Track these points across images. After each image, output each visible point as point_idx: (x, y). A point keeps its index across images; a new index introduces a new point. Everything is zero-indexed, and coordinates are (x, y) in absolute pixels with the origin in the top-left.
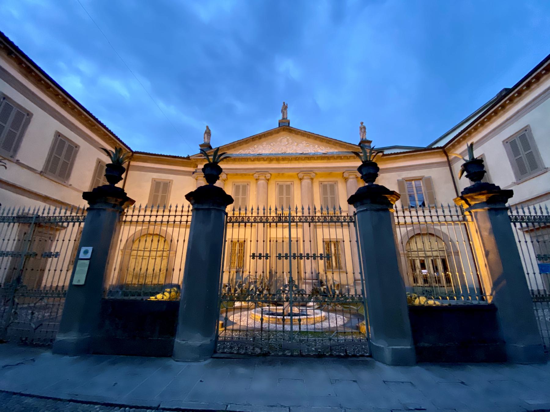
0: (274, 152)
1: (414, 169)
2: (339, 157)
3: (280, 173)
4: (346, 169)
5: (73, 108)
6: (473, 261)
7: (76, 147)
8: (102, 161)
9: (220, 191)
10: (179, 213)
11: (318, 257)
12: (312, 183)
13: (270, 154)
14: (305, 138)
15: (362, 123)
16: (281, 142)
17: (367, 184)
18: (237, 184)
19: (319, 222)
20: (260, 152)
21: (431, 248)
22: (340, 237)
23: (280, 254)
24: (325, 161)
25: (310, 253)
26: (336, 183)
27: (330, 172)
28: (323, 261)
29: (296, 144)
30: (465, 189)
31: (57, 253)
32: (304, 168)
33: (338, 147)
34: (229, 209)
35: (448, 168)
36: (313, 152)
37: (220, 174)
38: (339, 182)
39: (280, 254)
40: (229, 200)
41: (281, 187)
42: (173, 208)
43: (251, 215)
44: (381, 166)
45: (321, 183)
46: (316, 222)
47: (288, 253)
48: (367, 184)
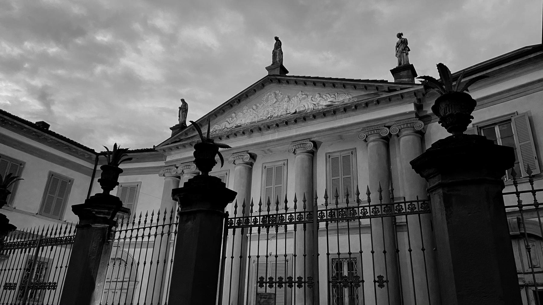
0: (256, 120)
1: (494, 103)
2: (356, 107)
4: (364, 125)
6: (387, 300)
7: (21, 165)
8: (56, 173)
9: (218, 184)
10: (142, 226)
11: (285, 283)
13: (251, 123)
14: (300, 87)
15: (400, 35)
16: (267, 101)
19: (364, 217)
20: (238, 123)
21: (533, 267)
22: (355, 249)
23: (262, 278)
24: (328, 118)
25: (274, 277)
26: (353, 151)
27: (339, 135)
28: (385, 289)
29: (286, 99)
30: (121, 202)
33: (351, 91)
34: (229, 208)
35: (90, 178)
36: (311, 107)
38: (358, 150)
39: (290, 278)
41: (269, 171)
45: (328, 156)
46: (360, 218)
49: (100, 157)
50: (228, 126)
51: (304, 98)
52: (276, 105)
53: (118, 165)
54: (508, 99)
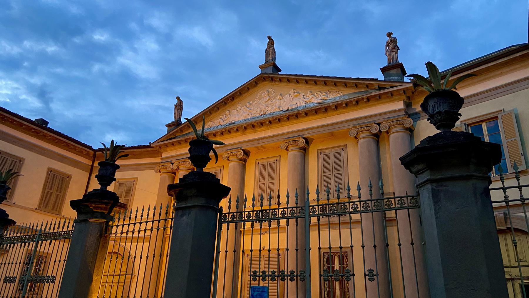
2: (347, 105)
3: (261, 146)
5: (12, 122)
7: (20, 161)
10: (138, 221)
12: (244, 166)
13: (245, 120)
17: (440, 131)
18: (262, 162)
19: (355, 212)
20: (232, 120)
21: (519, 261)
22: (346, 244)
26: (344, 148)
31: (54, 277)
32: (289, 133)
33: (342, 89)
34: (224, 203)
35: (88, 174)
36: (303, 104)
37: (460, 107)
39: (283, 272)
40: (225, 191)
41: (262, 167)
42: (133, 216)
43: (277, 206)
44: (463, 93)
45: (320, 152)
47: (295, 270)
48: (440, 131)
49: (97, 153)
50: (223, 123)
51: (296, 96)
52: (269, 102)
53: (115, 161)
54: (495, 96)
